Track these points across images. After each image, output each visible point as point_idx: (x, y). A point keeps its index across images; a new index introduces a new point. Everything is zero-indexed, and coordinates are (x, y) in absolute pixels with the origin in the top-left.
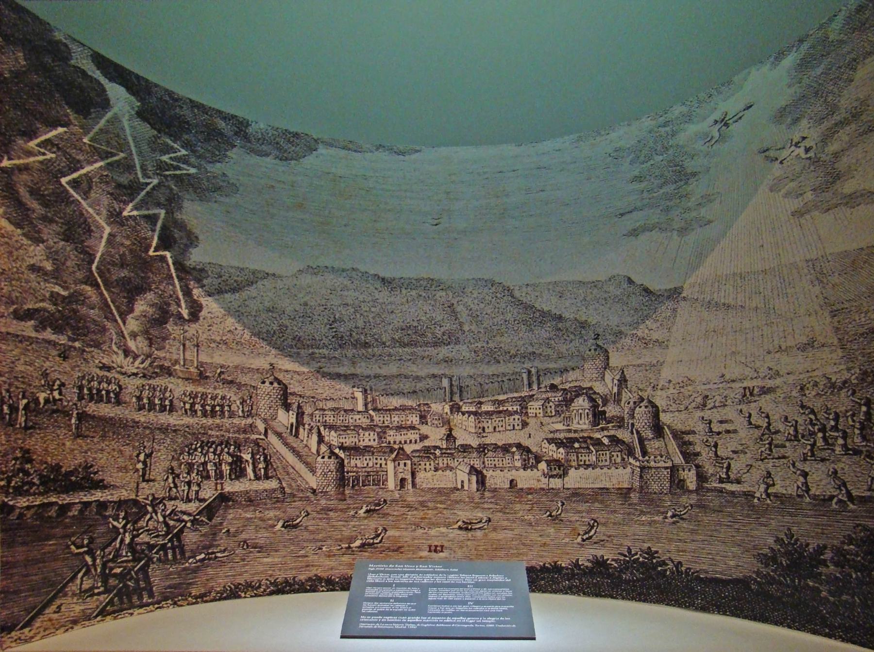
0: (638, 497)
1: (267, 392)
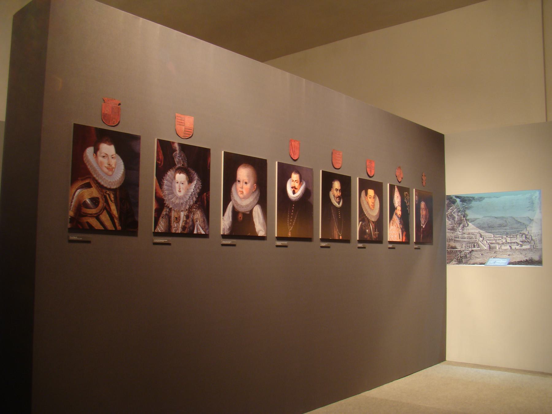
0: (530, 250)
1: (478, 235)
